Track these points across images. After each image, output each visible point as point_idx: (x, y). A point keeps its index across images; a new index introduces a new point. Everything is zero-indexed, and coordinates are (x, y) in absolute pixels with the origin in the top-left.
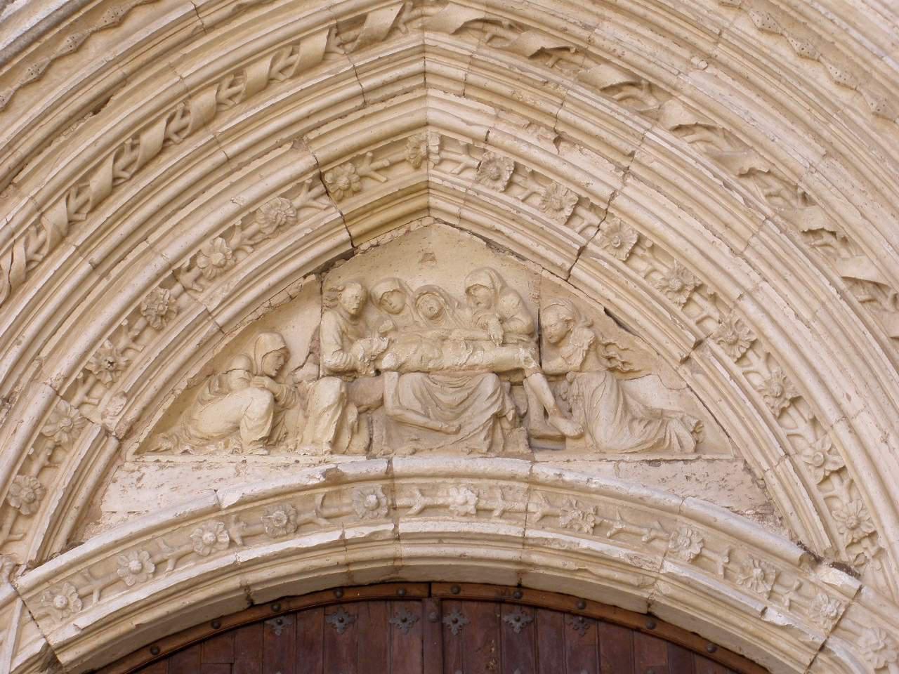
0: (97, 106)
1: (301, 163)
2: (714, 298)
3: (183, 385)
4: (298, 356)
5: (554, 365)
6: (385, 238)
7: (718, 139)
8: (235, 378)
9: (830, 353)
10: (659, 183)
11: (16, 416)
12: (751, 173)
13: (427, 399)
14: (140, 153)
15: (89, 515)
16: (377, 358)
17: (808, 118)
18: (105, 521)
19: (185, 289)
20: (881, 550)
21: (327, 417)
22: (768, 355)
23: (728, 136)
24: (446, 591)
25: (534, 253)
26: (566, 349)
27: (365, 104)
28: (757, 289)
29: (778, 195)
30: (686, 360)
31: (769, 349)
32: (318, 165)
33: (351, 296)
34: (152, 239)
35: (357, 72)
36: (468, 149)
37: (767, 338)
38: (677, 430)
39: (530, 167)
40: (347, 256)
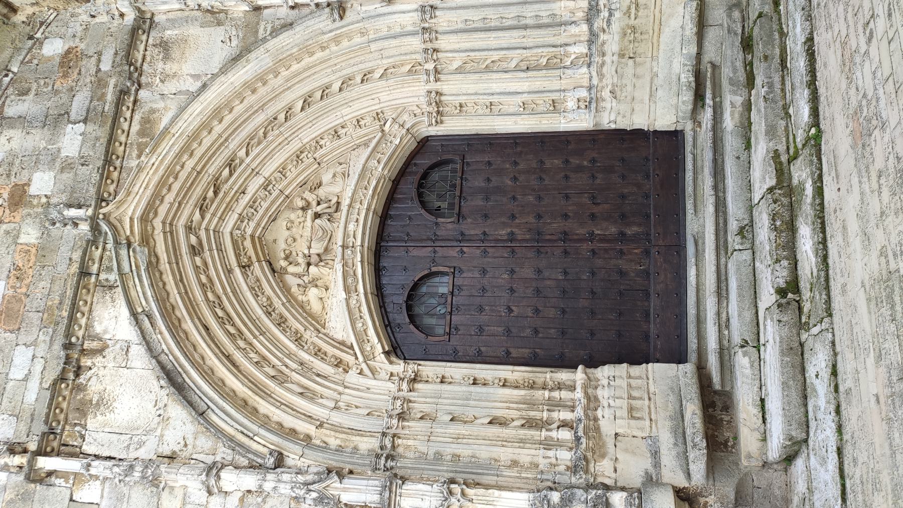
0: (207, 329)
1: (237, 271)
2: (301, 152)
3: (305, 314)
4: (301, 282)
5: (314, 203)
6: (266, 251)
7: (252, 142)
8: (304, 299)
9: (323, 119)
10: (262, 163)
11: (307, 362)
12: (265, 134)
13: (321, 239)
14: (225, 317)
15: (342, 343)
16: (305, 255)
17: (250, 113)
18: (345, 339)
19: (274, 311)
20: (382, 112)
21: (321, 270)
22: (321, 138)
23: (252, 139)
24: (379, 239)
25: (278, 207)
26: (310, 200)
27: (222, 251)
28: (300, 139)
29: (273, 127)
30: (319, 164)
31: (319, 138)
32: (239, 266)
33: (283, 263)
34: (255, 318)
35: (210, 250)
36: (242, 222)
37: (316, 137)
38: (339, 169)
39: (251, 203)
40: (271, 264)
